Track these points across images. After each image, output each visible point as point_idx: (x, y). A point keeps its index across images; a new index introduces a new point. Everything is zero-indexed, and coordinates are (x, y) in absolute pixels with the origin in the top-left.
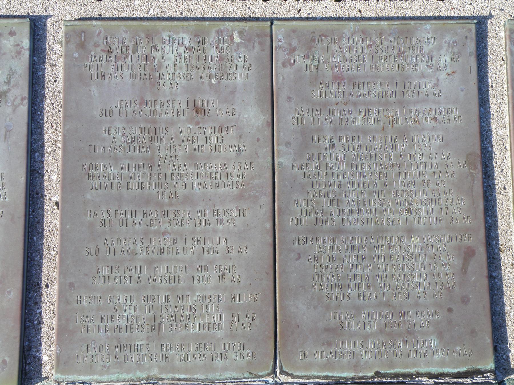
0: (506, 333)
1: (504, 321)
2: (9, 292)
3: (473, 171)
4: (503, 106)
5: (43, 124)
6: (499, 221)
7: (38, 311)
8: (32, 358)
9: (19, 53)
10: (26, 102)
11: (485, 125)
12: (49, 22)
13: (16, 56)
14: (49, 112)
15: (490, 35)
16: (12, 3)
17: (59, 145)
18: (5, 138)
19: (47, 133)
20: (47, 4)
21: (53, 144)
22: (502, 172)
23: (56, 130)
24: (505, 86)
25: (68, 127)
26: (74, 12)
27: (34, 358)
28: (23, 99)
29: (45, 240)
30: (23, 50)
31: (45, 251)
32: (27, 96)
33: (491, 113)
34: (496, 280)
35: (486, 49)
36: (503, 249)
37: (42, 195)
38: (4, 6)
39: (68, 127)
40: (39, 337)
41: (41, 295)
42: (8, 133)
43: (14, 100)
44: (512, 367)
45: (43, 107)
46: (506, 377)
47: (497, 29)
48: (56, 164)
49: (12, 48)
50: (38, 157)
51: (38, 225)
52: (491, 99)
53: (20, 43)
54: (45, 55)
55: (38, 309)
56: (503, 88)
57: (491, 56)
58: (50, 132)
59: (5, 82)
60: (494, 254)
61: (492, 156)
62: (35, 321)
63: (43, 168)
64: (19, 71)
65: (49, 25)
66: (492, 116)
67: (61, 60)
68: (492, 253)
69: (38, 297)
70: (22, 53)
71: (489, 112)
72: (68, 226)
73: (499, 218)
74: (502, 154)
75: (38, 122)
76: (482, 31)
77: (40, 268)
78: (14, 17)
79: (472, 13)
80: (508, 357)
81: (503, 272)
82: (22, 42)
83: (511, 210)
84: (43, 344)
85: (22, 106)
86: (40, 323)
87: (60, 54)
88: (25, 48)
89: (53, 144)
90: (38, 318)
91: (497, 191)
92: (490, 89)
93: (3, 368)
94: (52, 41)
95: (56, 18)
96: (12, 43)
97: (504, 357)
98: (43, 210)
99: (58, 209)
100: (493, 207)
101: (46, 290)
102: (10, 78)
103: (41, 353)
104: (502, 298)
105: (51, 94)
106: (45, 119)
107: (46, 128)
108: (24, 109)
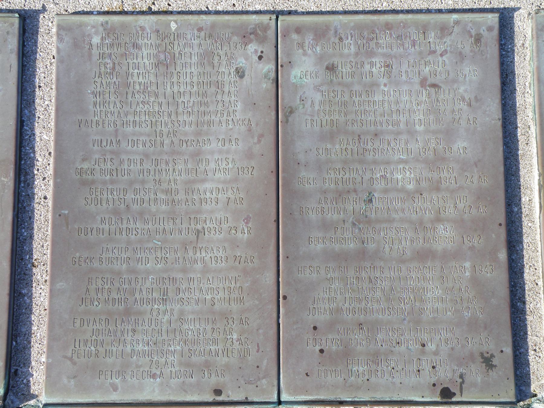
0: (30, 355)
1: (30, 342)
3: (4, 179)
4: (50, 108)
6: (35, 234)
11: (28, 129)
15: (42, 30)
22: (43, 180)
24: (54, 87)
33: (37, 116)
34: (26, 298)
35: (36, 46)
36: (37, 264)
44: (32, 392)
46: (23, 403)
47: (50, 24)
52: (37, 101)
56: (52, 89)
57: (41, 54)
60: (27, 270)
61: (33, 163)
66: (37, 119)
68: (24, 269)
71: (34, 115)
73: (35, 231)
74: (45, 160)
76: (33, 26)
79: (23, 6)
80: (29, 381)
81: (34, 289)
83: (50, 222)
91: (37, 201)
92: (37, 90)
97: (25, 381)
100: (30, 218)
104: (29, 317)
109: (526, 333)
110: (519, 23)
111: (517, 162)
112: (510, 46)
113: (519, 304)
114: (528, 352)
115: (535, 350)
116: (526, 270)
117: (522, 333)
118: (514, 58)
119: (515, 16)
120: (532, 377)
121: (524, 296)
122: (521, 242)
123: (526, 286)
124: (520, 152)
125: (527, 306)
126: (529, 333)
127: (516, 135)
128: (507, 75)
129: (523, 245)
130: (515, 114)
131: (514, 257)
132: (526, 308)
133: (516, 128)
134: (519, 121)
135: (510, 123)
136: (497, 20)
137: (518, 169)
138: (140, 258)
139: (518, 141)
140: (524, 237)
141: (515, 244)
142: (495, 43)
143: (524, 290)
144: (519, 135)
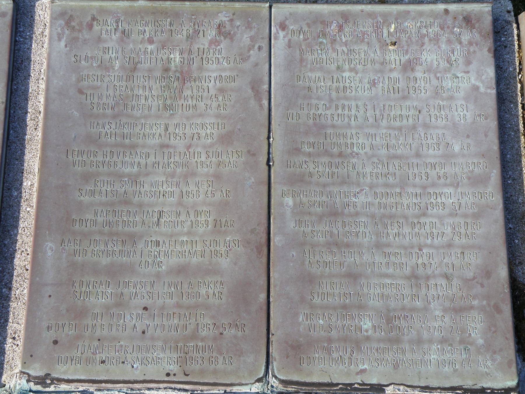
109: (7, 321)
110: (41, 12)
111: (23, 146)
112: (28, 34)
113: (4, 290)
114: (5, 341)
115: (14, 338)
116: (18, 255)
117: (2, 321)
118: (31, 45)
119: (37, 5)
120: (5, 366)
121: (11, 282)
122: (16, 227)
123: (15, 271)
124: (27, 137)
125: (13, 293)
126: (10, 320)
127: (25, 120)
128: (22, 61)
129: (18, 229)
130: (27, 100)
131: (6, 242)
132: (11, 295)
133: (27, 113)
134: (30, 106)
135: (20, 108)
136: (490, 9)
137: (23, 154)
138: (78, 250)
139: (27, 126)
140: (21, 222)
141: (9, 229)
142: (7, 28)
143: (13, 276)
144: (28, 119)
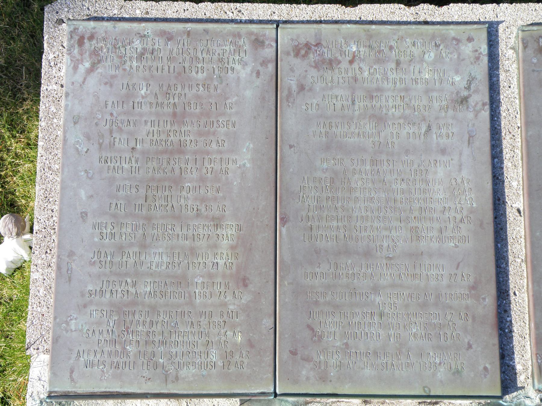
2: (484, 299)
5: (500, 130)
7: (508, 319)
8: (506, 367)
9: (478, 58)
10: (487, 107)
12: (501, 28)
13: (475, 62)
14: (505, 118)
16: (464, 10)
17: (518, 152)
18: (469, 143)
19: (504, 139)
20: (498, 10)
21: (511, 150)
23: (514, 136)
25: (530, 133)
26: (525, 18)
27: (508, 366)
28: (484, 105)
29: (509, 247)
30: (481, 55)
31: (511, 258)
32: (488, 102)
37: (503, 201)
38: (456, 13)
39: (530, 133)
40: (511, 345)
41: (510, 303)
42: (471, 139)
43: (476, 106)
45: (499, 113)
48: (516, 170)
49: (471, 54)
50: (498, 163)
51: (501, 232)
53: (478, 49)
54: (499, 61)
55: (508, 317)
58: (508, 138)
59: (465, 88)
62: (506, 329)
63: (503, 174)
64: (479, 77)
65: (501, 31)
67: (515, 66)
69: (507, 305)
70: (481, 58)
72: (538, 234)
75: (496, 128)
77: (507, 276)
78: (466, 23)
82: (480, 48)
84: (516, 353)
85: (483, 112)
86: (511, 331)
87: (513, 60)
88: (484, 53)
89: (511, 150)
90: (508, 326)
93: (485, 376)
94: (505, 46)
95: (507, 23)
96: (470, 49)
98: (505, 217)
99: (521, 216)
101: (514, 297)
102: (470, 83)
103: (514, 362)
105: (507, 99)
106: (503, 125)
107: (503, 134)
108: (486, 114)
